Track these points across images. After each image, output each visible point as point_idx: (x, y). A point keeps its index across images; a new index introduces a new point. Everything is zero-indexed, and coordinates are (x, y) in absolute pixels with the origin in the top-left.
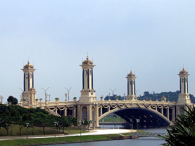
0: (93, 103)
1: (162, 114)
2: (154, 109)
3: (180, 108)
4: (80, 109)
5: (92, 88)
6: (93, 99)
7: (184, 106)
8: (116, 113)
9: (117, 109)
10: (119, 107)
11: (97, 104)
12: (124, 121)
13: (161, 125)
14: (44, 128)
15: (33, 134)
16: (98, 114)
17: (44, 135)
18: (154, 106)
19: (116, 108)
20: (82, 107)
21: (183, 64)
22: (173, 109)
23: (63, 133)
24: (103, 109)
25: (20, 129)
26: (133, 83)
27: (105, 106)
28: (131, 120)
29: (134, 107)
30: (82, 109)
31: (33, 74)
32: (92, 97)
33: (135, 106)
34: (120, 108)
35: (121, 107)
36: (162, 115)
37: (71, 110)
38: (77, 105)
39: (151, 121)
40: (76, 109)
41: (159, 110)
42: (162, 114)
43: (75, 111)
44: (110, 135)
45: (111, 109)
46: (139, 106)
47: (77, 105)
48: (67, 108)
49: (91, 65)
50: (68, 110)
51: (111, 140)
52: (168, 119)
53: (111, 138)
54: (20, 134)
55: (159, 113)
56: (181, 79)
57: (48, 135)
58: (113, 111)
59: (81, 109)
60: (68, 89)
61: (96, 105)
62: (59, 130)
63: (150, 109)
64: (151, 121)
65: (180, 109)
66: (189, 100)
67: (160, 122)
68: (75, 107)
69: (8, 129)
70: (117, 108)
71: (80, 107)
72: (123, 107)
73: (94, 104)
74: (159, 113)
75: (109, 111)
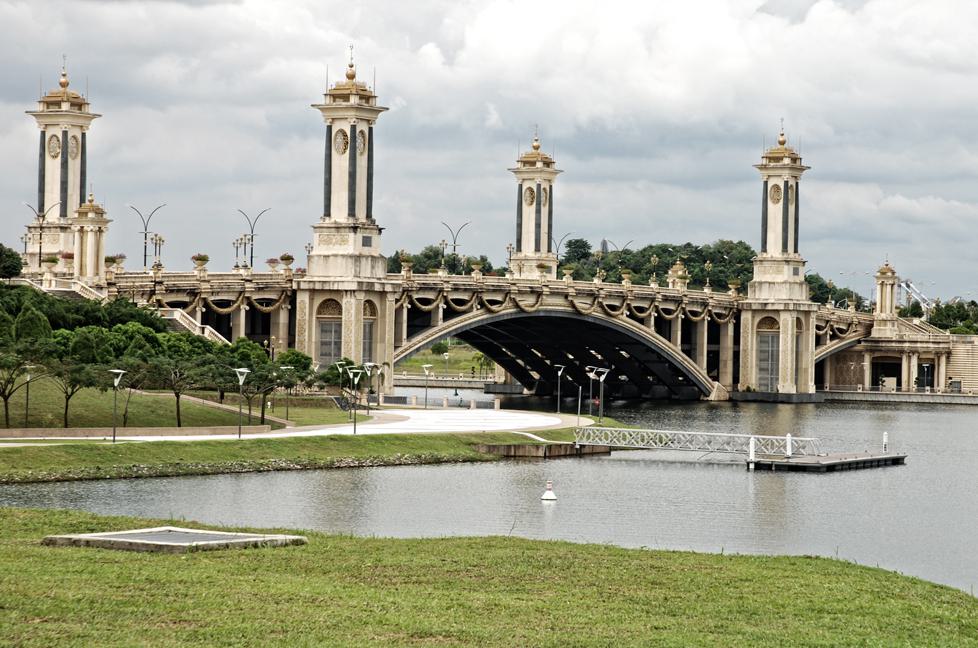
0: (373, 283)
1: (676, 345)
2: (641, 321)
3: (758, 319)
4: (307, 311)
5: (369, 215)
6: (373, 267)
7: (778, 311)
8: (466, 336)
9: (475, 317)
10: (482, 304)
11: (388, 288)
12: (499, 374)
13: (669, 398)
14: (178, 397)
15: (126, 421)
16: (390, 336)
17: (179, 426)
18: (641, 310)
19: (470, 310)
20: (318, 301)
21: (782, 120)
22: (726, 324)
23: (263, 421)
24: (414, 313)
25: (68, 399)
26: (543, 199)
27: (455, 301)
28: (560, 369)
29: (550, 311)
30: (319, 312)
31: (371, 129)
32: (367, 257)
33: (555, 305)
34: (490, 311)
35: (494, 308)
36: (674, 348)
37: (267, 316)
38: (294, 292)
39: (623, 378)
40: (290, 310)
41: (663, 327)
42: (676, 345)
43: (283, 317)
44: (483, 435)
45: (449, 314)
46: (573, 306)
47: (294, 292)
48: (250, 304)
49: (345, 104)
50: (252, 314)
51: (487, 461)
52: (699, 369)
53: (489, 452)
54: (67, 422)
55: (660, 341)
56: (524, 188)
57: (197, 429)
58: (457, 323)
59: (752, 324)
60: (146, 215)
61: (383, 294)
62: (245, 411)
63: (623, 320)
64: (623, 378)
65: (759, 326)
66: (801, 284)
67: (664, 384)
68: (284, 302)
69: (10, 394)
70: (475, 312)
71: (307, 300)
72: (506, 310)
73: (377, 288)
74: (660, 341)
75: (440, 322)
